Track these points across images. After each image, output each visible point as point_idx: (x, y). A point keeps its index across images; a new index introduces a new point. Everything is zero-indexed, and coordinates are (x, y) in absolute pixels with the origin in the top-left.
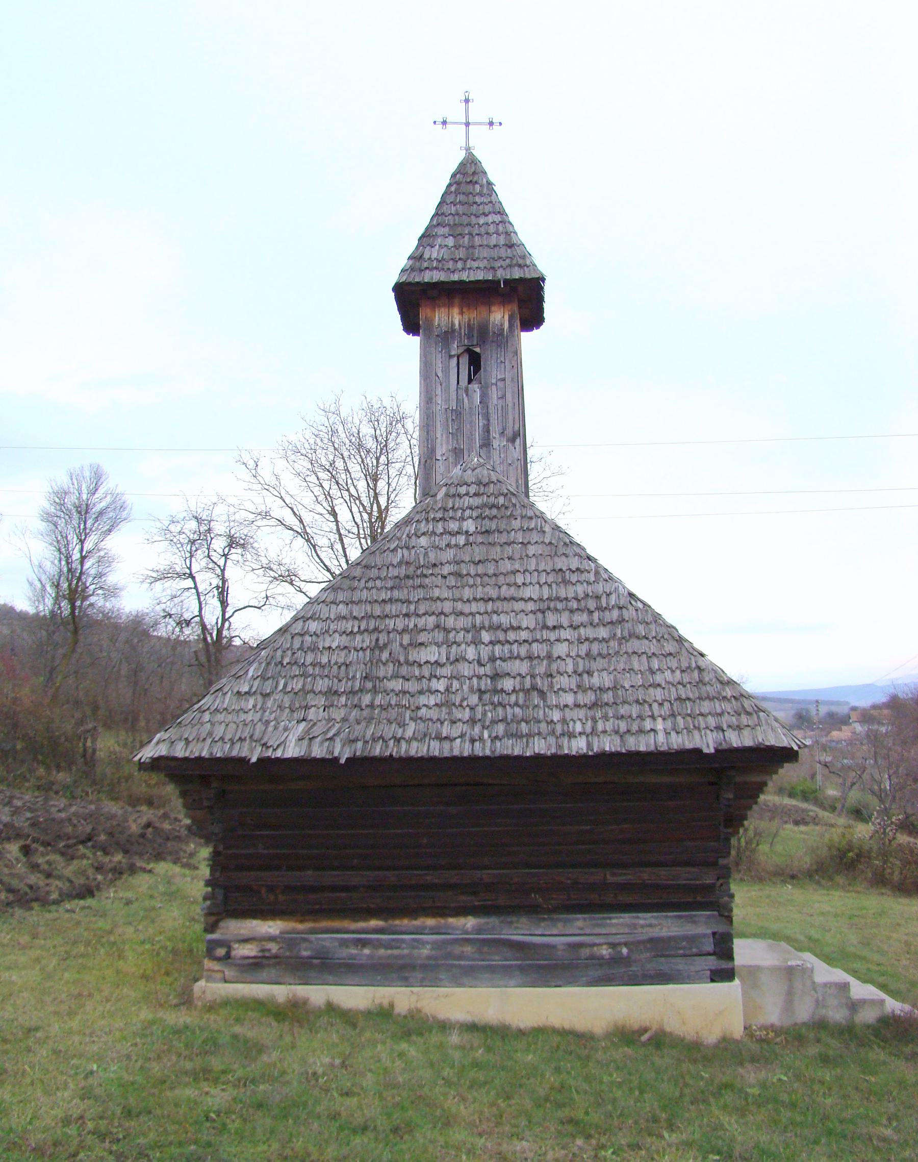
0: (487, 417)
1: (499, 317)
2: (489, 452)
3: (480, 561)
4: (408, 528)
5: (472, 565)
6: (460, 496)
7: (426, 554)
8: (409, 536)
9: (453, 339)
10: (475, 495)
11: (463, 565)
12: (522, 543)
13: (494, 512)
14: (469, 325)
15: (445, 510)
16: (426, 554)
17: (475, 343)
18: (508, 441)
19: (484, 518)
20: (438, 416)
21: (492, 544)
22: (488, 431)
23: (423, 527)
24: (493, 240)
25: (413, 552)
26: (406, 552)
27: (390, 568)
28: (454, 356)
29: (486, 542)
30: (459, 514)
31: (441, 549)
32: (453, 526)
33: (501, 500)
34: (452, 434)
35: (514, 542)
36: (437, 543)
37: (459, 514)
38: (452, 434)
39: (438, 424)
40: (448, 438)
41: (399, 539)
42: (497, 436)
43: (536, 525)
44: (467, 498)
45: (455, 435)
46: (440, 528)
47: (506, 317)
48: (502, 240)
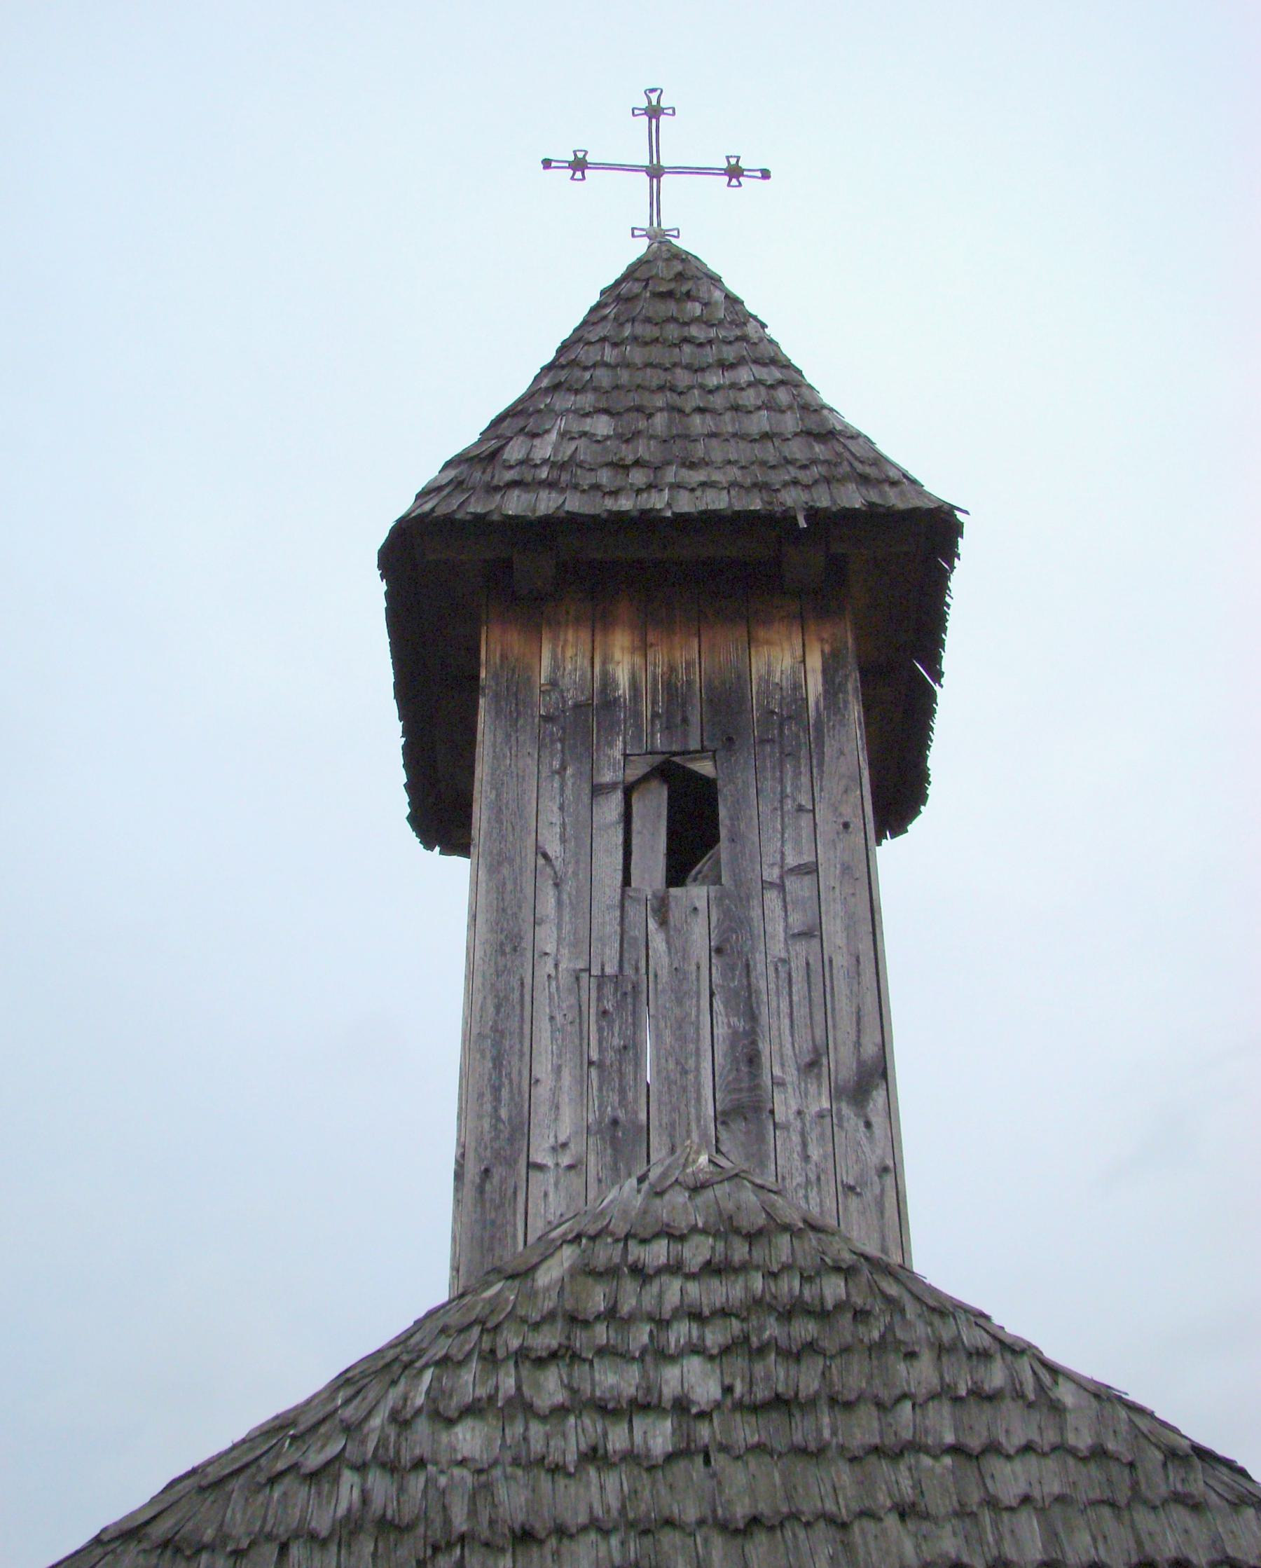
0: (747, 1005)
1: (790, 661)
2: (761, 1138)
3: (755, 1520)
4: (394, 1394)
5: (718, 1541)
6: (639, 1272)
7: (483, 1490)
8: (400, 1420)
9: (610, 729)
10: (712, 1269)
11: (669, 1539)
12: (956, 1450)
13: (805, 1329)
14: (670, 687)
15: (575, 1320)
16: (483, 1490)
17: (694, 745)
18: (837, 1094)
19: (761, 1351)
20: (542, 998)
21: (813, 1454)
22: (753, 1060)
23: (469, 1383)
24: (761, 422)
25: (417, 1483)
26: (379, 1483)
27: (296, 1551)
28: (613, 786)
29: (780, 1445)
30: (642, 1335)
31: (557, 1470)
32: (616, 1380)
33: (833, 1289)
34: (600, 1065)
35: (915, 1447)
36: (537, 1446)
37: (642, 1335)
38: (600, 1065)
39: (544, 1030)
40: (582, 1082)
41: (349, 1429)
42: (791, 1076)
43: (1013, 1377)
44: (676, 1284)
45: (613, 1068)
46: (550, 1387)
47: (815, 662)
48: (790, 423)
